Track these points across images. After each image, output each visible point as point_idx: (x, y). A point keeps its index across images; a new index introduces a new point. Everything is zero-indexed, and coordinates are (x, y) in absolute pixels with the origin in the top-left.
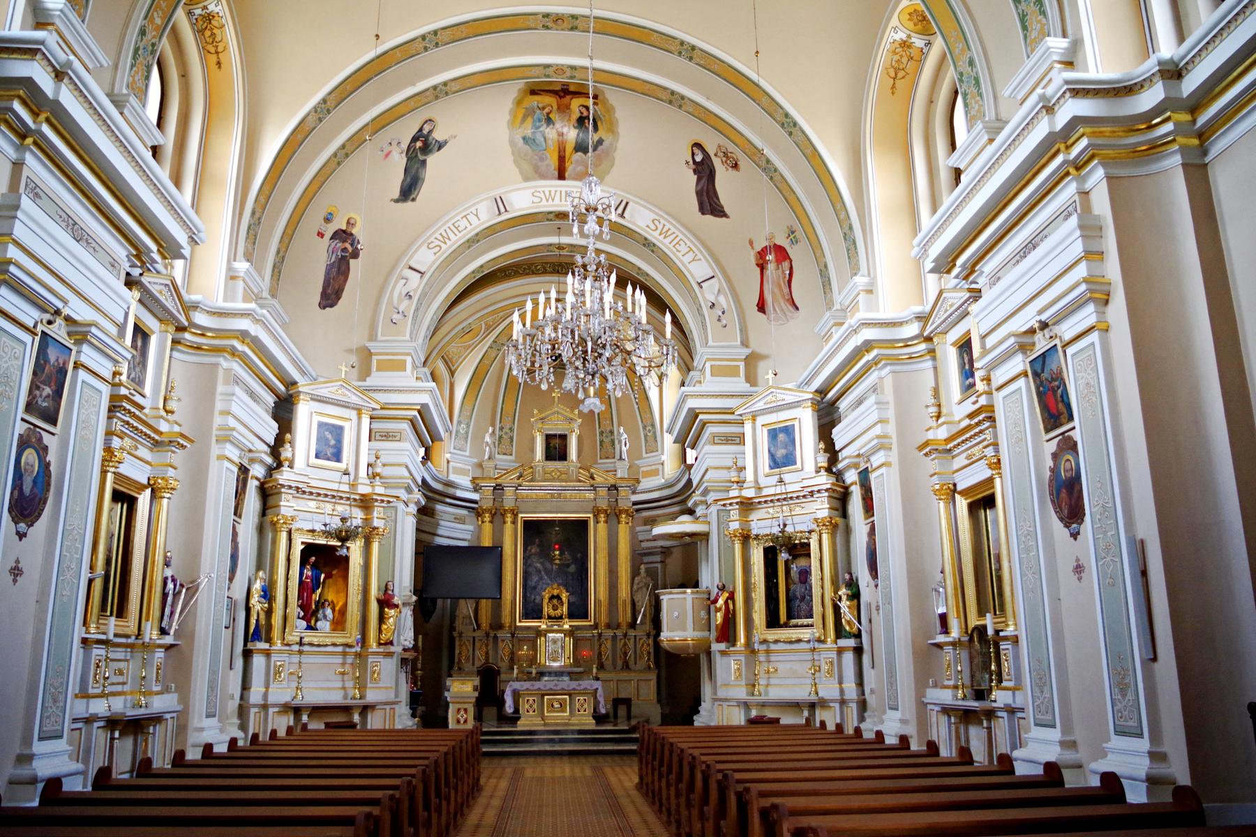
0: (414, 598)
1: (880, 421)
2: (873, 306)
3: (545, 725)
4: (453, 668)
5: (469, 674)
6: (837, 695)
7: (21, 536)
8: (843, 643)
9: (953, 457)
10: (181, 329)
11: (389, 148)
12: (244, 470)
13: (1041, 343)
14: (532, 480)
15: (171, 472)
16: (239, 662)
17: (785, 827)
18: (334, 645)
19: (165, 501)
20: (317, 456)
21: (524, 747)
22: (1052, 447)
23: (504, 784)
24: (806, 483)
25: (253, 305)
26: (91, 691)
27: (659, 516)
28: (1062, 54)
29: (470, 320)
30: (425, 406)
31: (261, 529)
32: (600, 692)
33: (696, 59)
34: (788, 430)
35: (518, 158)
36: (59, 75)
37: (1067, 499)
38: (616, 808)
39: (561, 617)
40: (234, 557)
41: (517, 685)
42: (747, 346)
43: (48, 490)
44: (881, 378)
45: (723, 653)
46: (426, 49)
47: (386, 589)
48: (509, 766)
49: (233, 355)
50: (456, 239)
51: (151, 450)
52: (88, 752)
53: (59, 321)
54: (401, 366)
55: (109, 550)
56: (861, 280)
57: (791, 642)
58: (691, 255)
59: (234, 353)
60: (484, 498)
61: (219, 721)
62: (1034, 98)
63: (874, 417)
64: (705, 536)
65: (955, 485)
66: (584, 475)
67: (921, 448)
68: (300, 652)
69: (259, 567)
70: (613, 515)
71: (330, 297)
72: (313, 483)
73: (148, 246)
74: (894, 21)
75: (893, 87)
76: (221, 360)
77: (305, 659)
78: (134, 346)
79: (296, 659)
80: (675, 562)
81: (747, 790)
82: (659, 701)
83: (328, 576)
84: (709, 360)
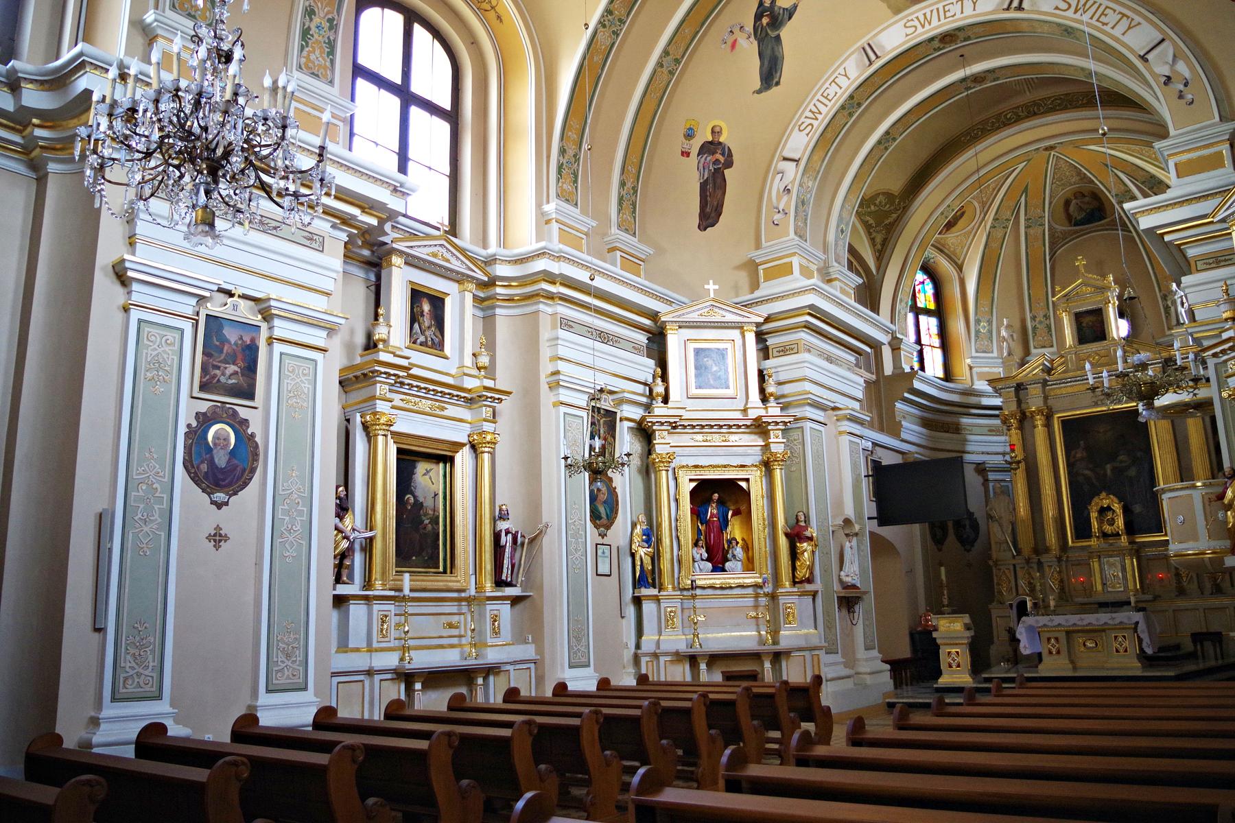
11: (733, 37)
16: (631, 611)
26: (375, 645)
29: (948, 202)
32: (1142, 627)
50: (827, 111)
54: (786, 270)
58: (1125, 23)
59: (551, 297)
71: (709, 215)
72: (686, 415)
76: (541, 307)
77: (698, 603)
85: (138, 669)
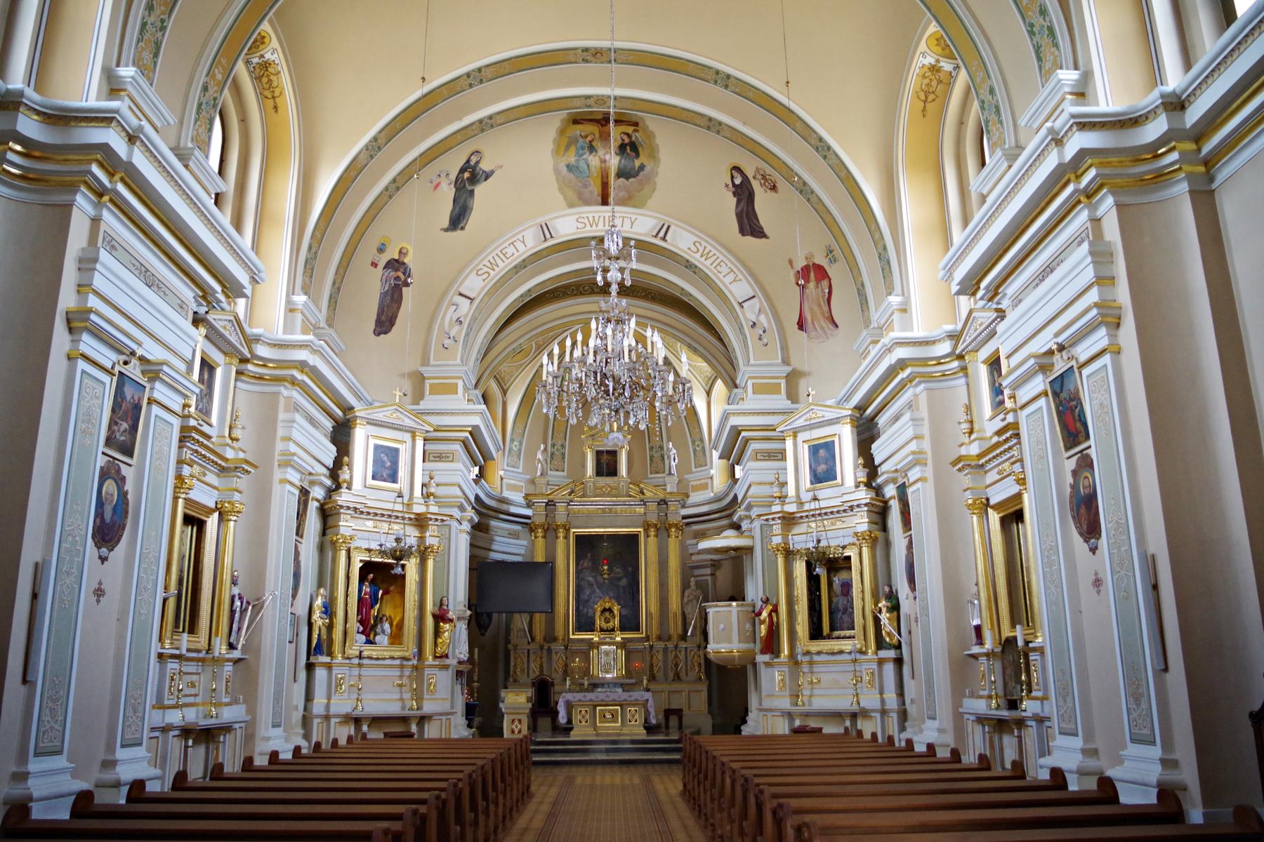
0: (469, 613)
1: (916, 437)
2: (908, 326)
3: (597, 735)
4: (508, 680)
5: (522, 686)
6: (876, 704)
7: (103, 559)
8: (884, 654)
9: (986, 472)
10: (244, 361)
12: (304, 493)
13: (1060, 365)
14: (583, 496)
15: (237, 496)
16: (302, 675)
17: (789, 825)
18: (392, 658)
19: (232, 523)
20: (374, 478)
21: (580, 756)
22: (1071, 464)
23: (554, 791)
24: (846, 498)
25: (310, 337)
26: (166, 702)
27: (708, 529)
28: (1073, 86)
29: (521, 341)
30: (476, 427)
31: (321, 549)
32: (651, 703)
33: (731, 87)
34: (829, 446)
35: (563, 185)
36: (132, 139)
37: (1085, 513)
38: (658, 813)
39: (613, 630)
40: (297, 576)
41: (569, 696)
42: (788, 364)
43: (126, 517)
44: (916, 395)
45: (767, 664)
46: (471, 86)
47: (441, 604)
48: (561, 774)
49: (293, 384)
50: (504, 266)
51: (218, 476)
52: (164, 758)
53: (134, 361)
54: (452, 389)
55: (181, 571)
56: (895, 300)
57: (833, 654)
58: (732, 276)
59: (294, 382)
60: (536, 514)
61: (285, 731)
62: (1043, 131)
63: (910, 433)
64: (750, 550)
65: (988, 499)
66: (634, 490)
67: (954, 463)
68: (360, 665)
69: (320, 584)
70: (663, 529)
71: (385, 323)
72: (370, 504)
73: (213, 286)
74: (923, 46)
75: (924, 110)
77: (364, 672)
78: (201, 380)
79: (356, 671)
80: (724, 575)
81: (761, 792)
82: (710, 712)
83: (386, 593)
84: (750, 378)
85: (52, 724)
